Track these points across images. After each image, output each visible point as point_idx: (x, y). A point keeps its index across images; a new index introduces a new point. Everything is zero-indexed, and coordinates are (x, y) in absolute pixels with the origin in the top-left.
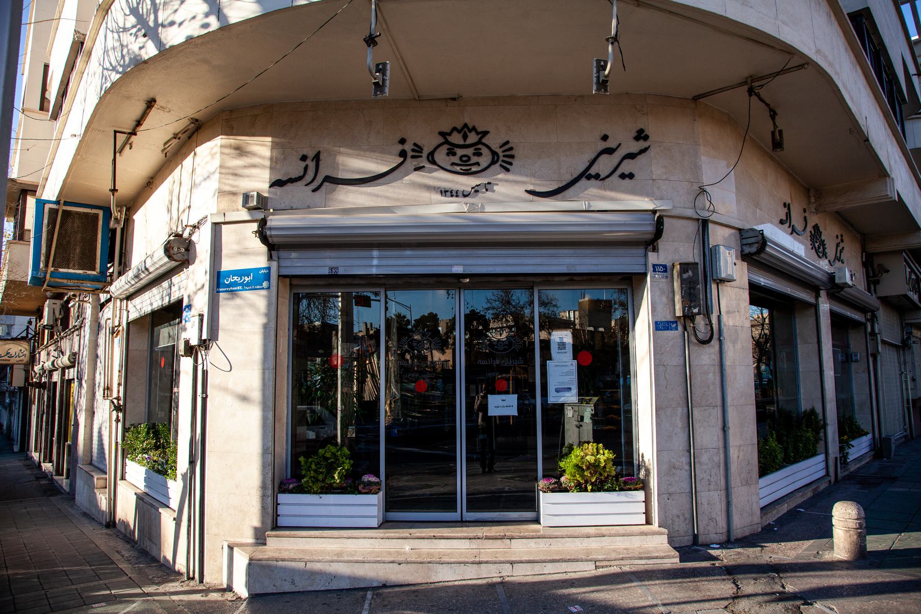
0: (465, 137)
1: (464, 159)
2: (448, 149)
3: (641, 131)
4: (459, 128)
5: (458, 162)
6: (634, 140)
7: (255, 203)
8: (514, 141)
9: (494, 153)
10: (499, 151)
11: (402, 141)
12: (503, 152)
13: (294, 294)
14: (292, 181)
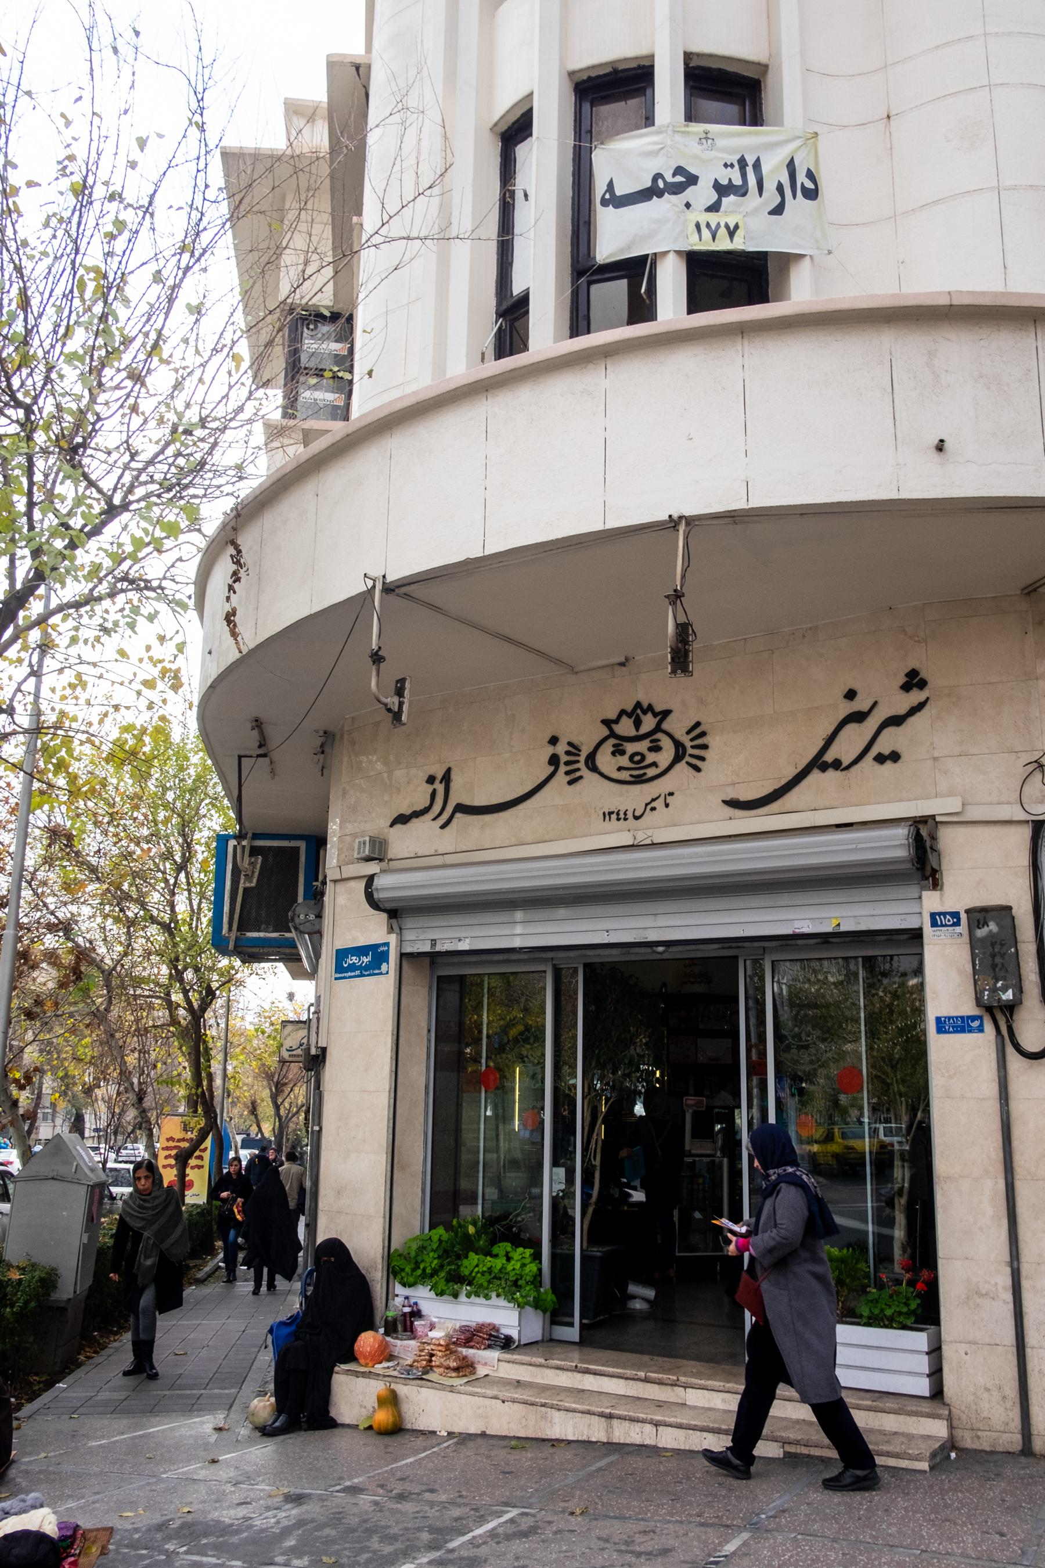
0: (638, 724)
1: (637, 758)
2: (614, 746)
3: (913, 674)
4: (629, 709)
5: (629, 765)
6: (901, 691)
7: (367, 852)
8: (707, 720)
9: (678, 745)
10: (585, 772)
11: (554, 741)
12: (692, 740)
13: (439, 977)
14: (417, 814)
